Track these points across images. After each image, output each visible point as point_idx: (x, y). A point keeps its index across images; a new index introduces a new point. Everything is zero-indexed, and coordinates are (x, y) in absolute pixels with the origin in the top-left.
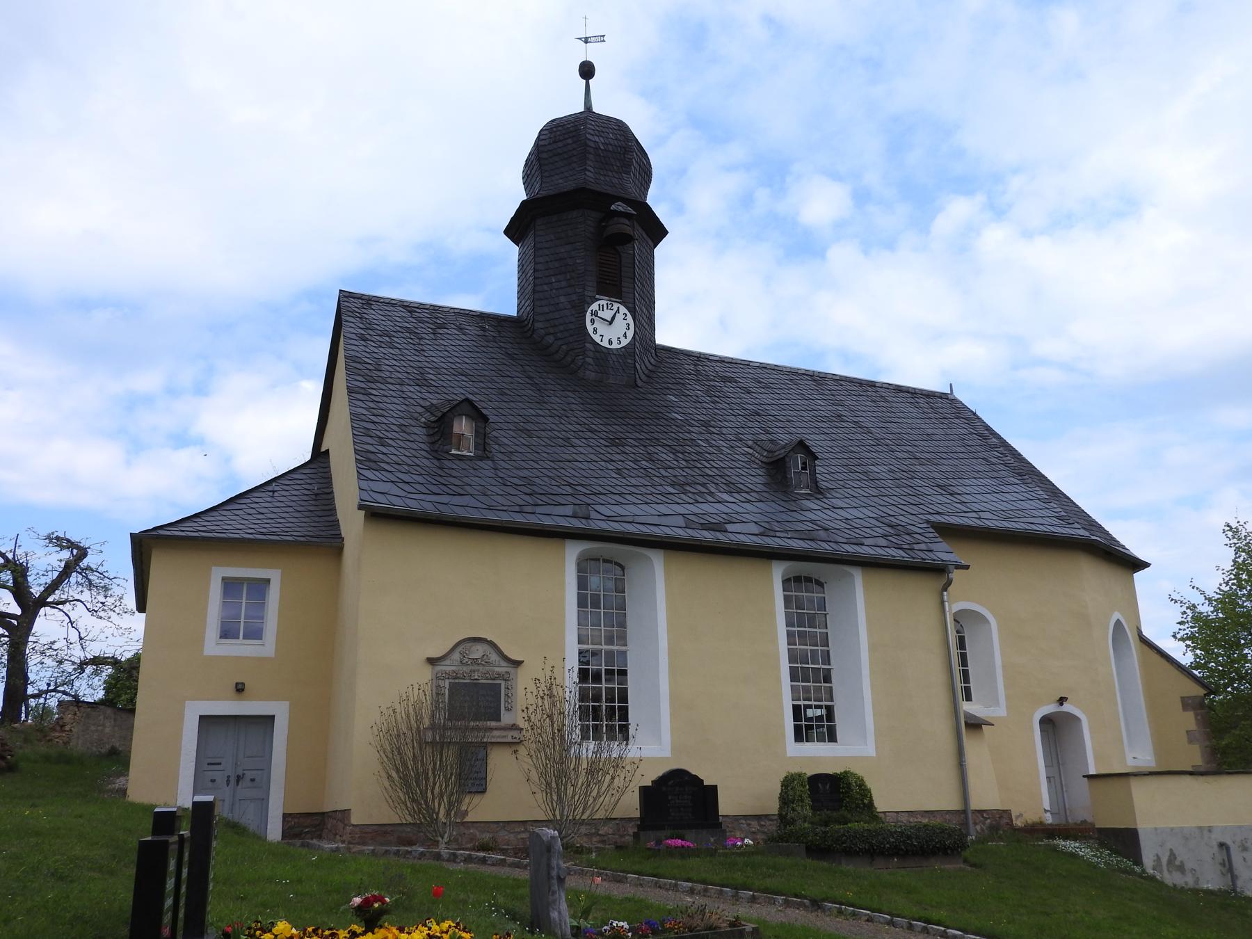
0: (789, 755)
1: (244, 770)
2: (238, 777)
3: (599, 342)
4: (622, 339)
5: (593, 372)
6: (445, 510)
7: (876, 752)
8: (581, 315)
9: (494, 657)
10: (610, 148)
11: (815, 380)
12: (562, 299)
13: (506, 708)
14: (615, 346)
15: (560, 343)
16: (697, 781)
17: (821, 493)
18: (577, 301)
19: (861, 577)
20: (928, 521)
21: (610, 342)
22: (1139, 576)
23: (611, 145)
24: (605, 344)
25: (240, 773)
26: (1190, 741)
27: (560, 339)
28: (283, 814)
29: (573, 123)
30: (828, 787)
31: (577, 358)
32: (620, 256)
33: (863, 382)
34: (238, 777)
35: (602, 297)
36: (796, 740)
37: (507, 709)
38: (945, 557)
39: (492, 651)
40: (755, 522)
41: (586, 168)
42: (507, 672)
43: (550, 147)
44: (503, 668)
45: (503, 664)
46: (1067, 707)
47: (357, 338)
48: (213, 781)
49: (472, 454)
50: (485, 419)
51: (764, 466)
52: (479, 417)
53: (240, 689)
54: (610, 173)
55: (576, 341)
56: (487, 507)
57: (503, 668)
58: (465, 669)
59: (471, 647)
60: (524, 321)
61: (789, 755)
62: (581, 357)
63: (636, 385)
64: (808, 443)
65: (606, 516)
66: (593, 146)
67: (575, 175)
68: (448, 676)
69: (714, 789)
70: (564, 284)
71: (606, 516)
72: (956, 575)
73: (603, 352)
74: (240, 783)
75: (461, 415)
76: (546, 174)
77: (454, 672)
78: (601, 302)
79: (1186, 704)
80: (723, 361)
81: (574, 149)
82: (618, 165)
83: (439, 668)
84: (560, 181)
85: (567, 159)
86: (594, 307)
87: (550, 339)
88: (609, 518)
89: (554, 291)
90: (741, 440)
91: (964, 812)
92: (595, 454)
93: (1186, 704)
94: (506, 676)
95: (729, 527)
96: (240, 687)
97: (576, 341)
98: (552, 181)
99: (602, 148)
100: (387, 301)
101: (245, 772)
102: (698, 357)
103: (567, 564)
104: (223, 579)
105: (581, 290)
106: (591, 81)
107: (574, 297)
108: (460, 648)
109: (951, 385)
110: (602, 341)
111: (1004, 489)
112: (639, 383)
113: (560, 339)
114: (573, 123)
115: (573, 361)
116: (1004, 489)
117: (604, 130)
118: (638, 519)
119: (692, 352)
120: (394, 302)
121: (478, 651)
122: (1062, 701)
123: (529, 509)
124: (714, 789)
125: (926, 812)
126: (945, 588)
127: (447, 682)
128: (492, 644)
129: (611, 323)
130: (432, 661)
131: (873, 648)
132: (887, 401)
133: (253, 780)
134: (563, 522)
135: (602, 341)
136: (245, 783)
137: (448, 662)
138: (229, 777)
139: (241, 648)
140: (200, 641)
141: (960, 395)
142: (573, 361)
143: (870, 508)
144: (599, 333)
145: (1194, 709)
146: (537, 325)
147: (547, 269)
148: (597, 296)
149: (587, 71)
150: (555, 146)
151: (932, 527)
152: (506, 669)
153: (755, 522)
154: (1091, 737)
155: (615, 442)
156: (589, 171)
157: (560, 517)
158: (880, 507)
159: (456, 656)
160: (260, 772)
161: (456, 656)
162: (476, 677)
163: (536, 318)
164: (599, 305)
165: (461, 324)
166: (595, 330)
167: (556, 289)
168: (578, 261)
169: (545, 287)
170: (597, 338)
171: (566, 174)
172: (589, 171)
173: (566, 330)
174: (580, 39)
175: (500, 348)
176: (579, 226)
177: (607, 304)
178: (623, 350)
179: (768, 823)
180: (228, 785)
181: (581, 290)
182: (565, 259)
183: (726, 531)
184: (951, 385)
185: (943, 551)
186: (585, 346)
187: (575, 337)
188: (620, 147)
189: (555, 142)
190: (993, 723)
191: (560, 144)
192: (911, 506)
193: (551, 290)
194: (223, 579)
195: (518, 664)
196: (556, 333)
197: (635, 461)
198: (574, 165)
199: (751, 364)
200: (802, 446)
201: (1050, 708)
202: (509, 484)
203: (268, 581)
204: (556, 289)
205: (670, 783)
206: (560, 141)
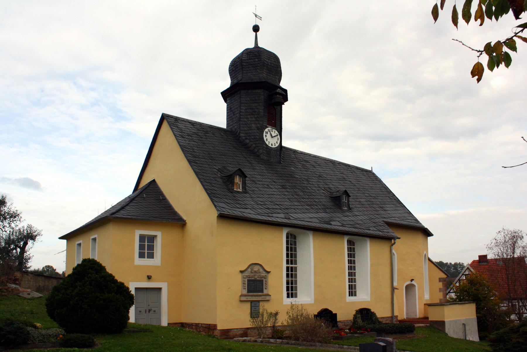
0: (347, 301)
1: (151, 307)
2: (149, 310)
3: (271, 146)
4: (276, 144)
5: (266, 156)
6: (246, 215)
7: (371, 300)
8: (262, 133)
9: (261, 270)
10: (272, 65)
11: (332, 163)
12: (253, 125)
13: (265, 288)
14: (273, 146)
15: (252, 143)
16: (331, 312)
17: (351, 210)
18: (260, 127)
19: (369, 240)
20: (384, 221)
21: (272, 145)
22: (429, 238)
23: (273, 64)
24: (270, 145)
25: (150, 308)
26: (440, 291)
27: (252, 142)
28: (168, 323)
29: (258, 52)
30: (365, 312)
31: (260, 150)
32: (276, 110)
33: (347, 165)
34: (149, 310)
35: (269, 126)
36: (349, 296)
37: (266, 289)
38: (393, 234)
39: (261, 268)
40: (338, 221)
41: (263, 72)
42: (266, 276)
43: (247, 61)
44: (264, 274)
45: (264, 272)
46: (413, 282)
47: (180, 136)
48: (140, 311)
49: (241, 191)
50: (246, 177)
51: (331, 198)
52: (243, 176)
53: (149, 278)
54: (272, 75)
55: (259, 143)
56: (257, 214)
57: (264, 274)
58: (252, 274)
59: (254, 266)
60: (234, 132)
61: (347, 301)
62: (261, 150)
63: (280, 163)
64: (348, 192)
65: (294, 218)
66: (266, 63)
67: (258, 74)
68: (247, 276)
69: (336, 314)
70: (254, 119)
71: (294, 218)
72: (397, 240)
73: (269, 149)
74: (150, 312)
75: (237, 175)
76: (245, 72)
77: (249, 275)
78: (269, 128)
79: (440, 280)
80: (302, 153)
81: (259, 63)
82: (275, 72)
83: (244, 274)
84: (252, 76)
85: (254, 67)
86: (266, 130)
87: (248, 141)
88: (296, 219)
89: (249, 122)
90: (320, 187)
91: (392, 317)
92: (279, 192)
93: (440, 280)
94: (265, 277)
95: (332, 223)
96: (150, 277)
97: (259, 143)
98: (248, 75)
99: (269, 64)
100: (183, 119)
101: (152, 308)
102: (294, 151)
103: (283, 235)
104: (140, 235)
105: (262, 123)
106: (258, 33)
107: (259, 125)
108: (251, 267)
109: (372, 167)
110: (269, 144)
111: (397, 208)
112: (282, 162)
113: (252, 142)
114: (258, 52)
115: (258, 151)
116: (397, 208)
117: (270, 57)
118: (306, 220)
119: (173, 116)
120: (185, 120)
121: (256, 268)
122: (412, 280)
123: (270, 215)
124: (336, 314)
125: (382, 317)
126: (392, 245)
127: (247, 279)
128: (261, 265)
129: (272, 137)
130: (242, 272)
131: (371, 266)
132: (355, 173)
133: (155, 311)
134: (279, 220)
135: (269, 144)
136: (152, 312)
137: (247, 272)
138: (146, 310)
139: (146, 262)
140: (133, 260)
141: (374, 171)
142: (258, 151)
143: (366, 216)
144: (268, 141)
145: (442, 281)
146: (242, 135)
147: (246, 112)
148: (268, 126)
149: (256, 29)
150: (250, 61)
151: (385, 223)
152: (265, 274)
153: (338, 221)
154: (418, 292)
155: (283, 187)
156: (264, 73)
157: (280, 218)
158: (368, 215)
159: (249, 270)
160: (157, 308)
161: (249, 270)
162: (256, 277)
163: (241, 132)
164: (268, 129)
165: (213, 132)
166: (267, 140)
167: (250, 121)
168: (260, 111)
169: (245, 120)
170: (267, 143)
171: (254, 73)
172: (264, 73)
173: (255, 138)
174: (254, 14)
175: (230, 144)
176: (261, 96)
177: (271, 129)
178: (276, 148)
179: (340, 323)
180: (146, 313)
181: (262, 123)
182: (255, 109)
183: (331, 224)
184: (372, 167)
185: (392, 232)
186: (263, 146)
187: (259, 141)
188: (276, 65)
189: (250, 59)
190: (398, 288)
191: (252, 60)
192: (280, 189)
193: (248, 121)
194: (140, 235)
195: (268, 272)
196: (250, 139)
197: (292, 195)
198: (258, 70)
199: (311, 155)
200: (346, 192)
201: (408, 283)
202: (259, 204)
203: (156, 236)
204: (250, 121)
205: (324, 313)
206: (252, 59)
